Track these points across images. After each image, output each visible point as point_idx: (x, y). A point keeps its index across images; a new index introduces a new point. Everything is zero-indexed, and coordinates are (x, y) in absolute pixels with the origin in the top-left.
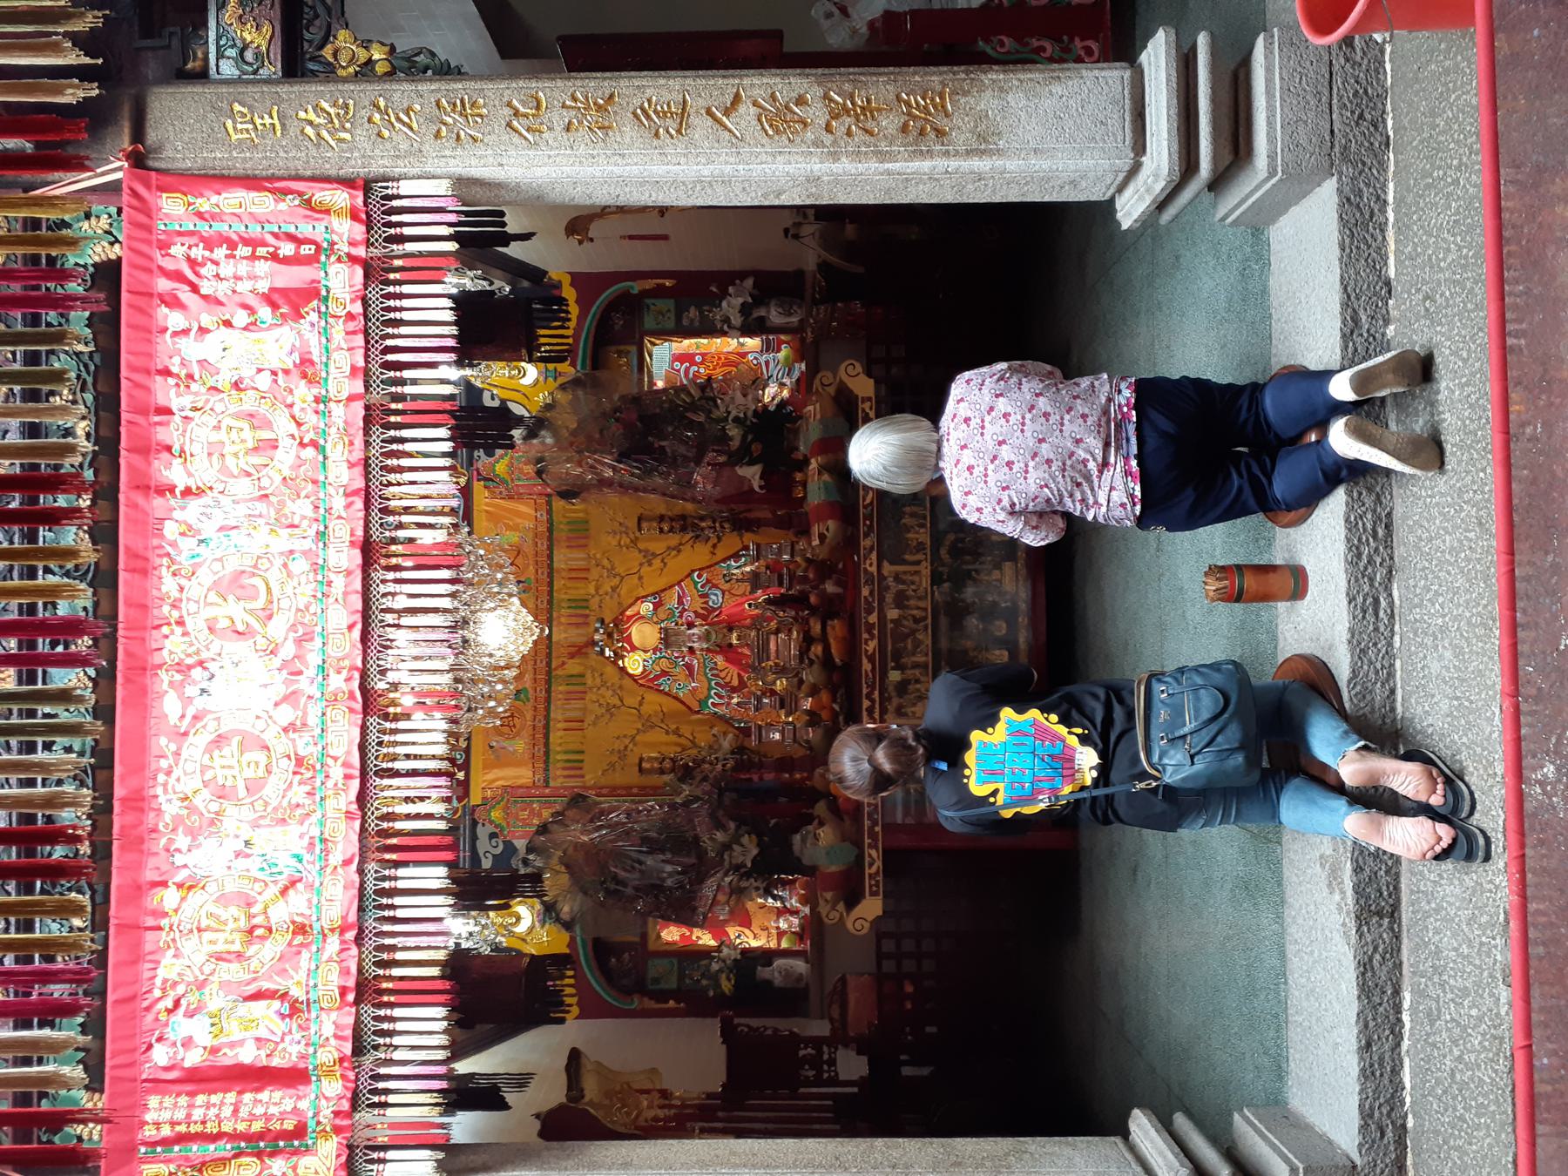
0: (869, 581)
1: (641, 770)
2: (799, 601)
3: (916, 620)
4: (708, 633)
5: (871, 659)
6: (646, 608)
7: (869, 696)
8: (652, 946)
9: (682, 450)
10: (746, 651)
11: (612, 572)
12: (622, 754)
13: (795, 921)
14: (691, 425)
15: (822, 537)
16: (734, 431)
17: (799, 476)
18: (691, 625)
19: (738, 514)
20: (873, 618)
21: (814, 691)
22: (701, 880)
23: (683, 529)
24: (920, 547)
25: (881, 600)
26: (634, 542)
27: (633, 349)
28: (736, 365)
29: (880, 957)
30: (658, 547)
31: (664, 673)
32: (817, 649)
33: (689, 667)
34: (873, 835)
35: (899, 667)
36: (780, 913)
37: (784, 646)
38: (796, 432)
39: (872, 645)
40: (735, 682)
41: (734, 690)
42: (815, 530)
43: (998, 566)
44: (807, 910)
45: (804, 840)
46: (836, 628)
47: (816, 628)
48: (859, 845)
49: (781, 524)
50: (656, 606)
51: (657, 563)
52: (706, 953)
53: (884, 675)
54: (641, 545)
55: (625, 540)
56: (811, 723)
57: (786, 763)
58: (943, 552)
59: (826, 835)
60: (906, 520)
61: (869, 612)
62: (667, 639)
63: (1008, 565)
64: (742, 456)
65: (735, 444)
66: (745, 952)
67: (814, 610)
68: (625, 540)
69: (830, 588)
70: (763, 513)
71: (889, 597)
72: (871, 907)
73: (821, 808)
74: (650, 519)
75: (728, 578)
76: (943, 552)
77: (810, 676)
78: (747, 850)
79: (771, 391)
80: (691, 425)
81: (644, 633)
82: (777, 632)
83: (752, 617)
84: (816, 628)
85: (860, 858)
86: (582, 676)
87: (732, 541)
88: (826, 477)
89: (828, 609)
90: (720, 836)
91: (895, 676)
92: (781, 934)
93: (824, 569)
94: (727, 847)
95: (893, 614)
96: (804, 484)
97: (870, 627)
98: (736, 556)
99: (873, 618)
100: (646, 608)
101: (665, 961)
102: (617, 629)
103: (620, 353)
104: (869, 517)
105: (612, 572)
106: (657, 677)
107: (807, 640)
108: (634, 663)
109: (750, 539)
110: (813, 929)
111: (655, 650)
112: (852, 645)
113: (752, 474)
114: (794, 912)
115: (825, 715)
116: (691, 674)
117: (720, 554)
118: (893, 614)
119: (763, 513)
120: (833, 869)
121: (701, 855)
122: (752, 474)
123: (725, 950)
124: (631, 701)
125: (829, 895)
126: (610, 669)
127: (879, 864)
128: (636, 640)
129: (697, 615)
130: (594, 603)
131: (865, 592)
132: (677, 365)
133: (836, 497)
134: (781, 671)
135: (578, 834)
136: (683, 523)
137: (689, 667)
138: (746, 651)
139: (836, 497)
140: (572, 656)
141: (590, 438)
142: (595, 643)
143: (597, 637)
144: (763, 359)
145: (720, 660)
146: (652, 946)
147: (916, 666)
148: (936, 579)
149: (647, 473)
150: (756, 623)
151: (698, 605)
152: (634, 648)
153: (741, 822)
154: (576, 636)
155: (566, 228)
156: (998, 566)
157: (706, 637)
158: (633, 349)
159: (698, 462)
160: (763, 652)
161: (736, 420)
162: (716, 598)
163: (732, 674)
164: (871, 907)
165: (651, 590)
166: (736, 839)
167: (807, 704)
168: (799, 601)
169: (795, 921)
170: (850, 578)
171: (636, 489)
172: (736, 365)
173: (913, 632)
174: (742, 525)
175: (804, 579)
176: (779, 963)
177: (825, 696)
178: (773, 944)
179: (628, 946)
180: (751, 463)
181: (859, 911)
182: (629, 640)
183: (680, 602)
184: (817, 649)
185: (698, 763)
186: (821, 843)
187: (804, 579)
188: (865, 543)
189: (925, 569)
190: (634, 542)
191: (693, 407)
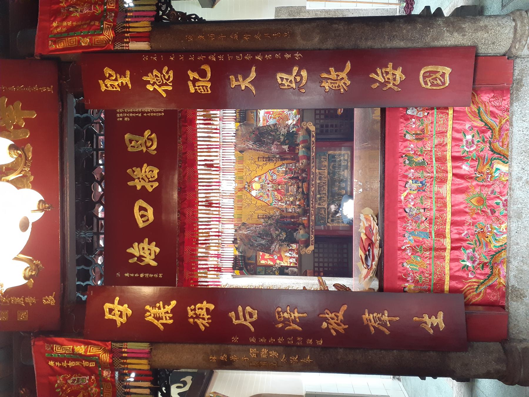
0: (313, 174)
1: (258, 218)
2: (297, 178)
3: (324, 183)
4: (273, 186)
5: (313, 192)
6: (257, 179)
7: (312, 201)
8: (258, 264)
9: (269, 141)
10: (283, 191)
11: (249, 170)
12: (252, 216)
13: (294, 260)
14: (271, 135)
15: (302, 163)
16: (282, 137)
17: (297, 147)
18: (268, 184)
19: (282, 156)
20: (313, 183)
21: (299, 200)
22: (272, 243)
23: (269, 160)
24: (325, 166)
25: (316, 178)
26: (255, 162)
27: (255, 111)
28: (281, 114)
29: (314, 257)
30: (261, 163)
31: (261, 196)
32: (301, 190)
33: (267, 195)
34: (312, 232)
35: (319, 194)
36: (291, 258)
37: (293, 189)
38: (297, 137)
39: (313, 189)
40: (280, 199)
41: (279, 201)
42: (301, 161)
43: (343, 171)
44: (297, 256)
45: (296, 234)
46: (305, 185)
47: (300, 184)
48: (309, 234)
49: (292, 159)
50: (259, 179)
51: (260, 168)
52: (272, 266)
53: (316, 195)
54: (257, 163)
55: (253, 162)
56: (299, 208)
57: (292, 217)
58: (331, 167)
59: (302, 232)
60: (322, 160)
61: (313, 181)
62: (262, 187)
63: (346, 171)
64: (284, 143)
65: (282, 140)
66: (281, 266)
67: (300, 180)
68: (253, 162)
69: (304, 175)
70: (288, 156)
71: (318, 178)
72: (311, 248)
73: (301, 227)
74: (261, 158)
75: (278, 171)
76: (331, 167)
77: (298, 197)
78: (284, 236)
79: (290, 122)
80: (271, 135)
81: (256, 186)
82: (291, 185)
83: (285, 182)
84: (300, 184)
85: (309, 237)
86: (241, 196)
87: (280, 163)
88: (303, 149)
89: (303, 180)
90: (277, 232)
91: (318, 196)
92: (291, 263)
93: (303, 171)
94: (278, 235)
95: (318, 181)
96: (299, 149)
97: (313, 184)
98: (281, 166)
99: (313, 183)
100: (257, 179)
101: (261, 268)
102: (250, 183)
103: (251, 112)
104: (313, 159)
105: (249, 170)
106: (259, 197)
107: (298, 187)
108: (254, 193)
109: (285, 162)
110: (299, 260)
111: (259, 190)
112: (308, 189)
113: (286, 147)
114: (294, 258)
115: (302, 205)
116: (268, 197)
117: (277, 166)
118: (318, 181)
119: (288, 156)
120: (303, 239)
121: (272, 238)
122: (286, 147)
123: (277, 265)
124: (254, 202)
125: (302, 245)
126: (248, 194)
127: (313, 238)
128: (254, 188)
129: (270, 181)
130: (245, 177)
131: (312, 176)
132: (266, 114)
133: (305, 154)
134: (292, 195)
135: (244, 232)
136: (269, 159)
137: (267, 195)
138: (283, 191)
139: (305, 154)
140: (239, 191)
141: (247, 138)
142: (245, 188)
143: (246, 186)
144: (289, 113)
145: (276, 193)
146: (258, 264)
147: (323, 194)
148: (329, 173)
149: (261, 146)
150: (286, 183)
151: (270, 178)
152: (253, 190)
153: (282, 229)
154: (241, 186)
155: (422, 379)
156: (343, 171)
157: (273, 187)
158: (255, 111)
159: (273, 143)
160: (287, 191)
161: (282, 135)
162: (275, 177)
163: (279, 197)
164: (311, 248)
165: (259, 175)
166: (281, 233)
167: (298, 203)
168: (297, 178)
169: (294, 260)
170: (308, 174)
171: (258, 151)
172: (281, 114)
173: (323, 186)
174: (283, 159)
175: (298, 173)
176: (290, 269)
177: (302, 201)
178: (289, 265)
179: (251, 264)
180: (286, 145)
181: (308, 248)
182: (252, 187)
183: (266, 178)
184: (301, 190)
185: (272, 216)
186: (301, 234)
187: (298, 173)
188: (312, 165)
189: (326, 171)
190: (255, 162)
191: (272, 131)
